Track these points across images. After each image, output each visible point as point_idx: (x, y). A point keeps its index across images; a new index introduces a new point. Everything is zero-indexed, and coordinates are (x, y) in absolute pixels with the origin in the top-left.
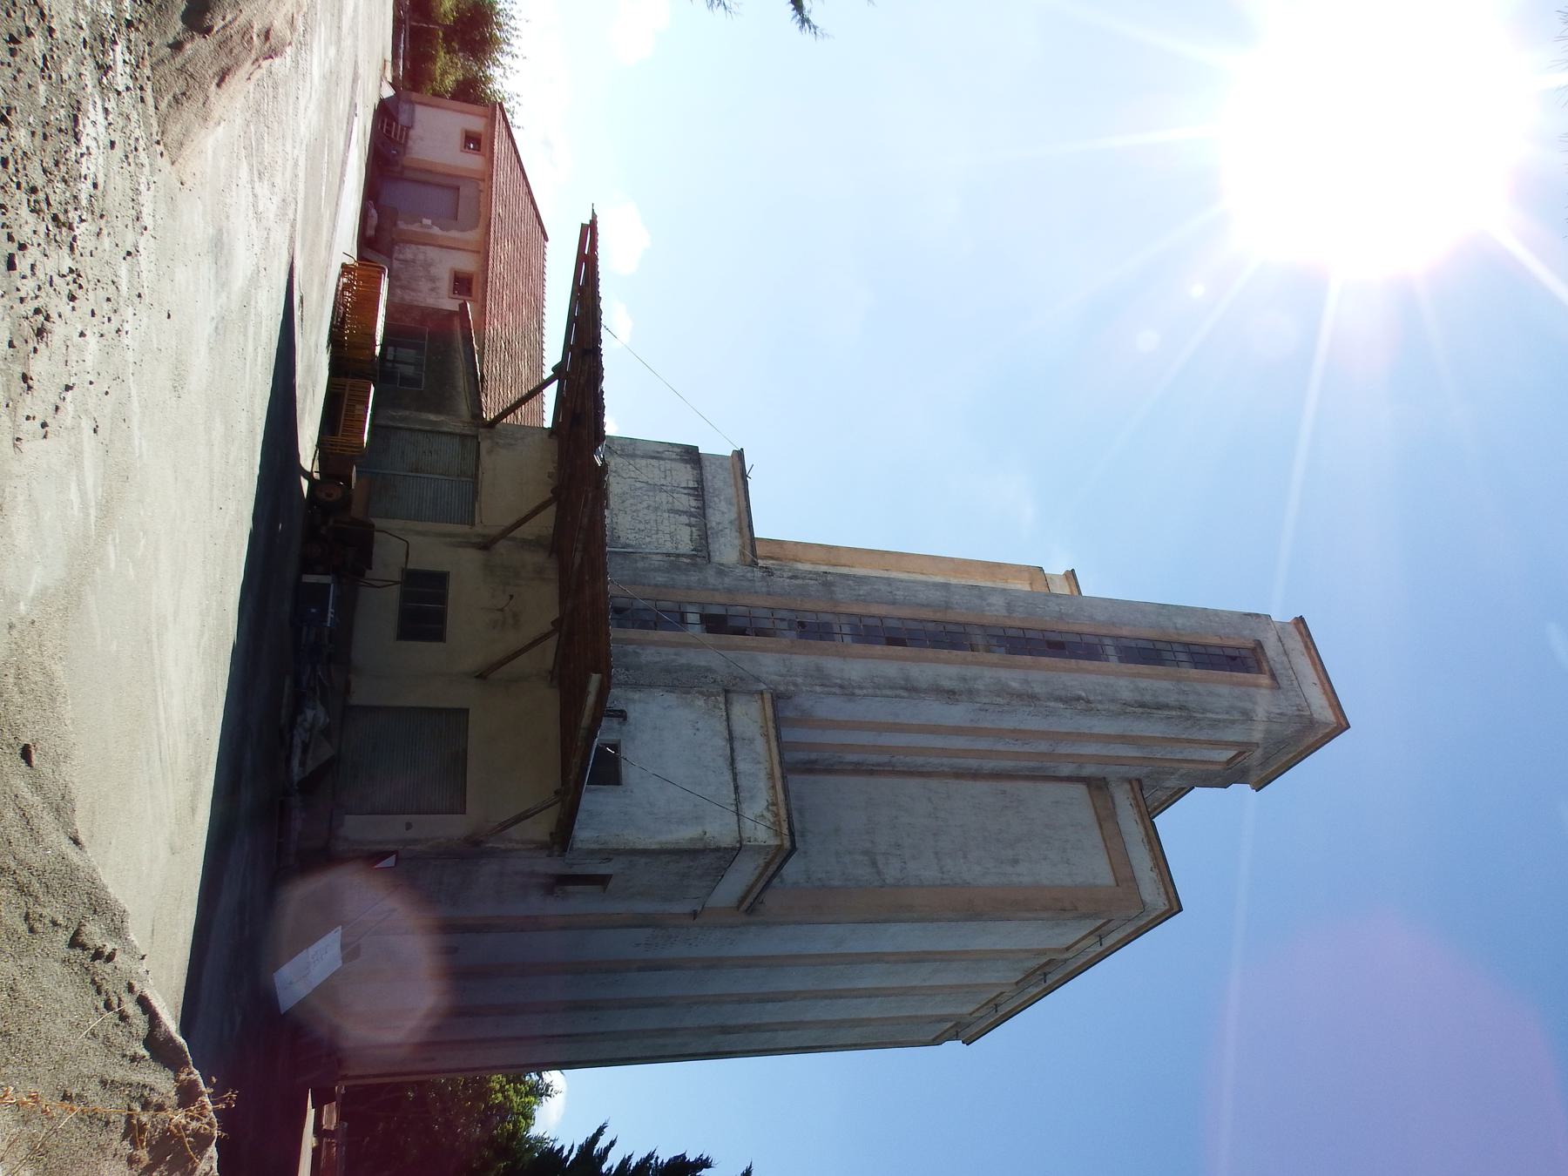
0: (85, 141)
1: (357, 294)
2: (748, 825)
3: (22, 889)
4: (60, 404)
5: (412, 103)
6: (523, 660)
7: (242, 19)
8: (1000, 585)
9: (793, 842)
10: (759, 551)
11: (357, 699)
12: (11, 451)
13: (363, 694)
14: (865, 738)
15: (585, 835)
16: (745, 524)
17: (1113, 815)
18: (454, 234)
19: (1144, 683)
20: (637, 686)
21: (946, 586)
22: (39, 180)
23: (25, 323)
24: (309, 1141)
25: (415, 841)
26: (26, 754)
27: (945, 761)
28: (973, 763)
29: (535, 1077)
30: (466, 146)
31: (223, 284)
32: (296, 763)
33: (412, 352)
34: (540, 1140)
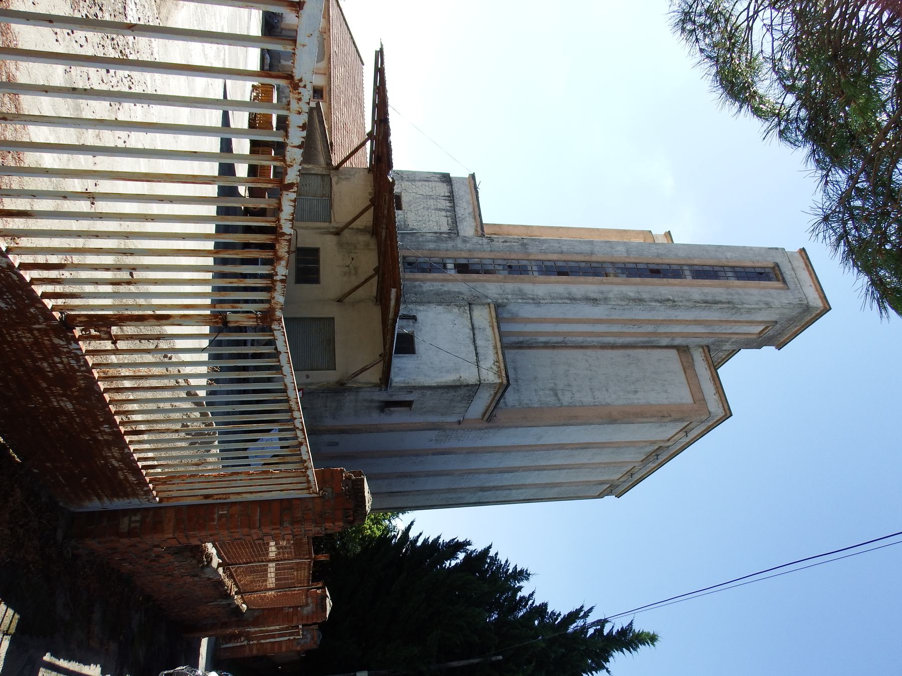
2: (484, 372)
9: (508, 380)
10: (486, 230)
14: (549, 328)
15: (397, 379)
16: (477, 214)
17: (692, 366)
19: (706, 290)
20: (421, 303)
21: (591, 242)
25: (311, 384)
27: (595, 339)
28: (611, 340)
29: (387, 522)
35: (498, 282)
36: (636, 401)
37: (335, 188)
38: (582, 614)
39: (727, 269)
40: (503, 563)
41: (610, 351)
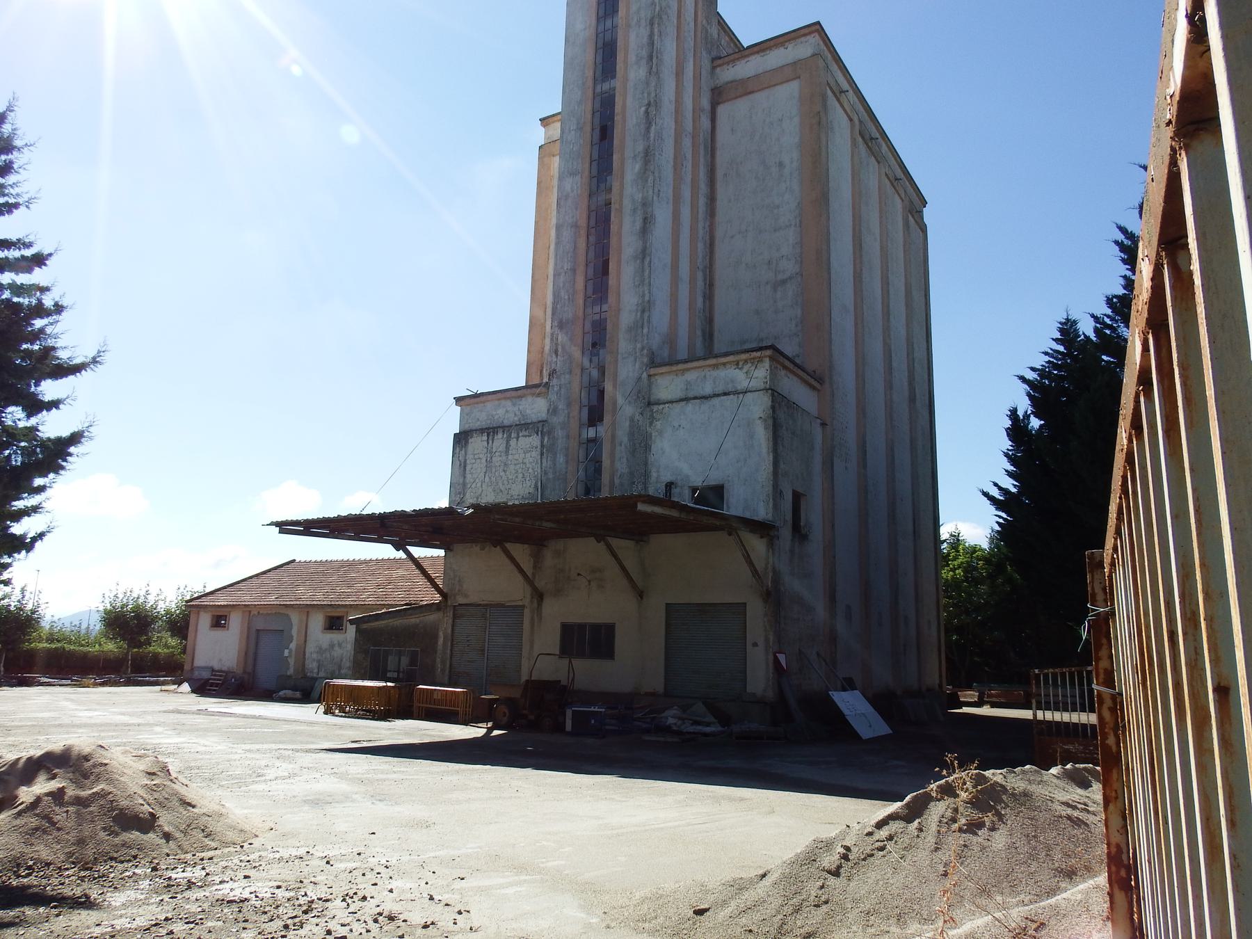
0: (246, 895)
1: (347, 702)
2: (755, 384)
3: (797, 910)
4: (443, 903)
5: (192, 669)
6: (628, 564)
7: (142, 792)
8: (555, 182)
9: (767, 348)
10: (537, 381)
11: (658, 685)
12: (479, 934)
13: (656, 683)
15: (762, 512)
16: (514, 394)
18: (294, 632)
19: (632, 58)
20: (646, 475)
22: (278, 924)
23: (385, 928)
24: (986, 711)
25: (767, 640)
26: (700, 912)
27: (701, 225)
28: (702, 201)
29: (945, 545)
30: (223, 626)
31: (347, 798)
32: (708, 730)
33: (390, 658)
34: (992, 540)
35: (616, 361)
36: (795, 164)
37: (473, 599)
38: (1126, 242)
39: (601, 28)
40: (1047, 358)
41: (718, 203)
